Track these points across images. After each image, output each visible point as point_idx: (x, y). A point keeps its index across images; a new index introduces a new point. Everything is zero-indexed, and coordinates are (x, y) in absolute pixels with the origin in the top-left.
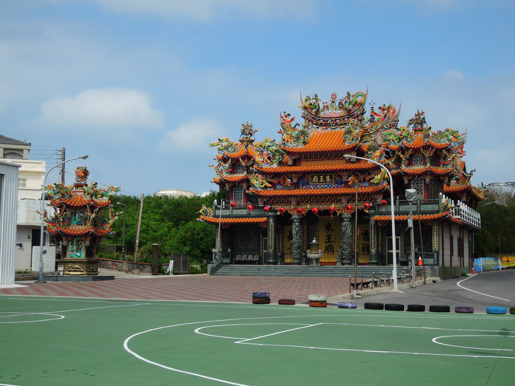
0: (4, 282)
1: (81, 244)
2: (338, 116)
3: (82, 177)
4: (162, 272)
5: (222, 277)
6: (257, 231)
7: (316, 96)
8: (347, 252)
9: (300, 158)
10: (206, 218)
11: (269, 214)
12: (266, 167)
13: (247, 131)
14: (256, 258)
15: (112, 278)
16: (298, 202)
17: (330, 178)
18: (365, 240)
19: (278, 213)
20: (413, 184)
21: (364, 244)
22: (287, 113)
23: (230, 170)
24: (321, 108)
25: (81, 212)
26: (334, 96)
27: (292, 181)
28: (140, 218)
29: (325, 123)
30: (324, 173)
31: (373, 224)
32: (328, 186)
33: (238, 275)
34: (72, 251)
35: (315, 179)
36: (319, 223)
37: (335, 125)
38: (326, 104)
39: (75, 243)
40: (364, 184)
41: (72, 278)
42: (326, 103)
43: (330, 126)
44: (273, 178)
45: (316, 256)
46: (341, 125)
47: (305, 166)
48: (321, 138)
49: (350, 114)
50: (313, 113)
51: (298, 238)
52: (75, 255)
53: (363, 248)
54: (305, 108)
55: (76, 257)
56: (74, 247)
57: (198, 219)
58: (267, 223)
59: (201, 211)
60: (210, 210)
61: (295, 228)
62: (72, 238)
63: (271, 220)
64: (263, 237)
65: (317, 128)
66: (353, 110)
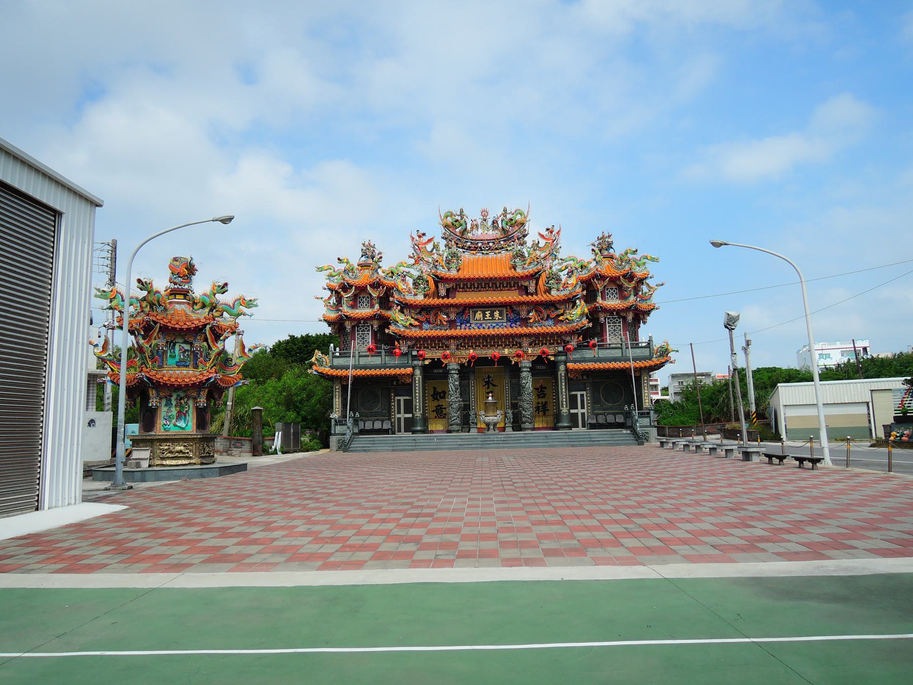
0: (57, 500)
1: (187, 403)
3: (184, 276)
4: (266, 452)
5: (362, 454)
7: (462, 211)
10: (321, 369)
12: (410, 298)
14: (387, 426)
15: (243, 467)
17: (501, 315)
19: (427, 362)
22: (421, 232)
24: (469, 227)
25: (186, 342)
27: (448, 317)
29: (475, 247)
34: (168, 418)
35: (479, 315)
36: (490, 371)
39: (174, 403)
40: (547, 323)
41: (162, 474)
44: (420, 313)
46: (497, 249)
47: (462, 298)
48: (473, 265)
49: (508, 237)
50: (456, 231)
51: (458, 395)
52: (175, 425)
53: (537, 409)
55: (177, 429)
56: (173, 409)
57: (309, 371)
58: (412, 375)
59: (313, 359)
60: (326, 358)
62: (168, 389)
63: (418, 372)
64: (396, 395)
66: (511, 231)
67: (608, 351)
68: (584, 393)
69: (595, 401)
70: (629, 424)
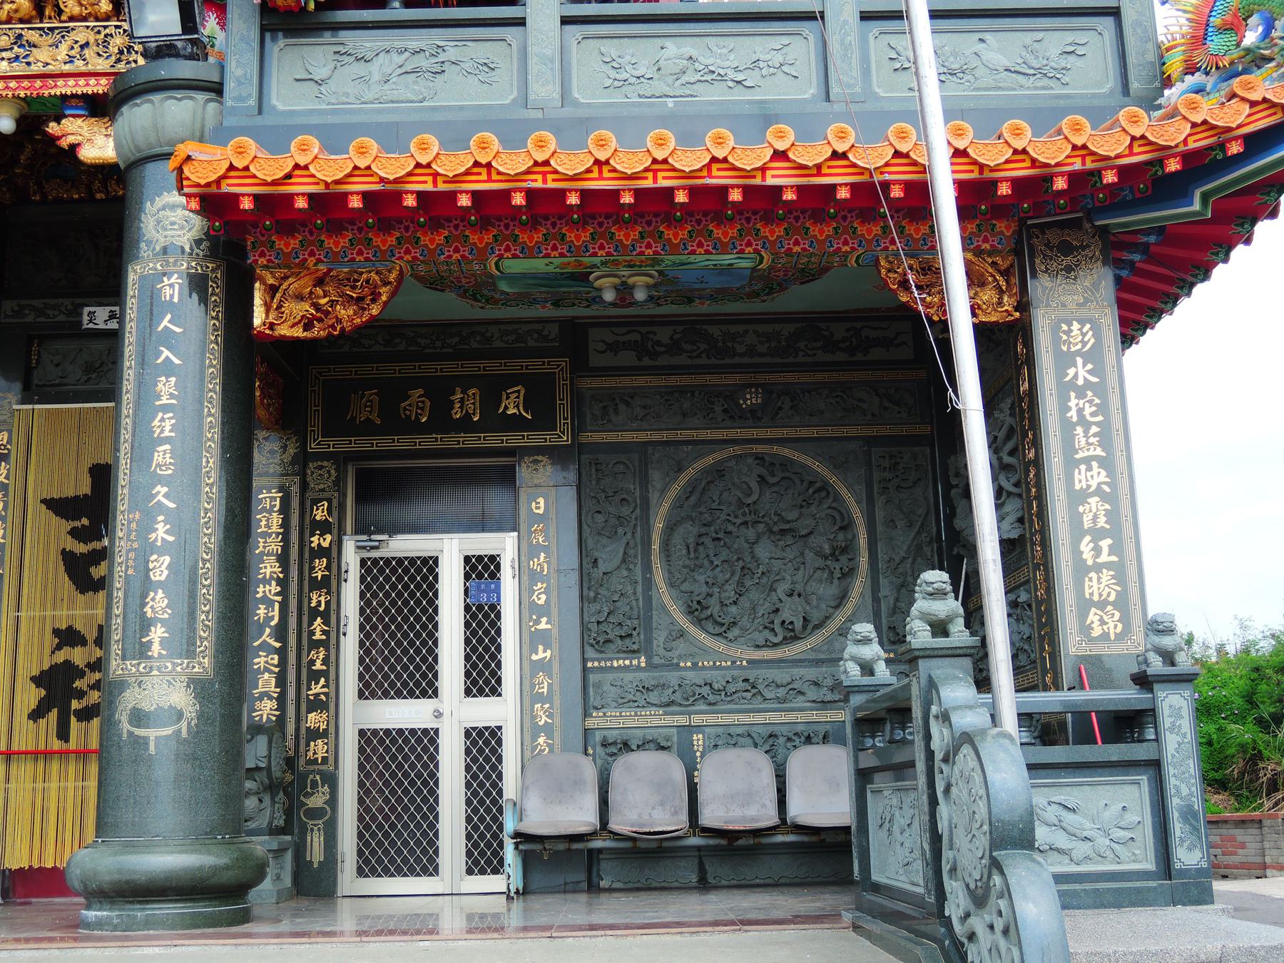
67: (676, 49)
68: (505, 545)
69: (607, 624)
70: (894, 861)
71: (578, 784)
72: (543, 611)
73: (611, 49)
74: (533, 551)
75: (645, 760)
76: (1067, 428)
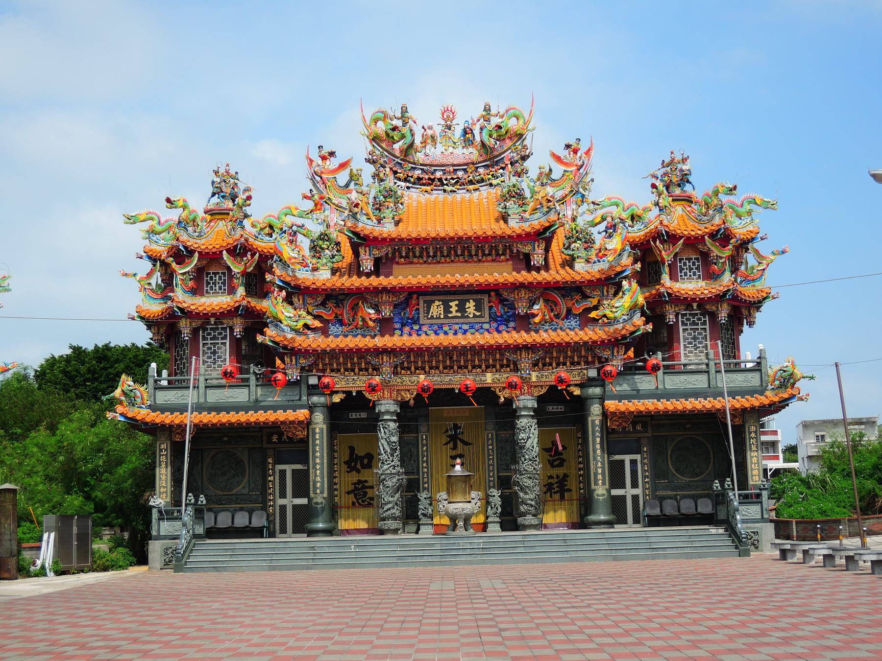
2: (462, 161)
6: (288, 443)
7: (404, 110)
8: (532, 497)
9: (394, 254)
11: (315, 399)
12: (304, 276)
13: (227, 190)
14: (258, 520)
16: (396, 367)
18: (553, 466)
19: (337, 399)
20: (683, 324)
21: (551, 477)
23: (191, 284)
24: (418, 140)
26: (448, 115)
28: (177, 378)
29: (429, 179)
30: (462, 292)
31: (597, 422)
32: (472, 327)
33: (262, 568)
35: (436, 309)
36: (458, 420)
37: (456, 183)
38: (430, 132)
40: (566, 323)
42: (430, 128)
43: (443, 184)
44: (323, 304)
45: (468, 508)
46: (471, 182)
47: (404, 277)
49: (491, 158)
50: (395, 150)
54: (375, 139)
58: (307, 424)
59: (117, 393)
61: (388, 435)
63: (319, 418)
65: (408, 188)
66: (498, 151)
67: (683, 377)
68: (638, 457)
69: (658, 473)
70: (722, 516)
71: (656, 506)
72: (647, 471)
73: (672, 377)
74: (645, 458)
75: (669, 501)
76: (750, 445)
